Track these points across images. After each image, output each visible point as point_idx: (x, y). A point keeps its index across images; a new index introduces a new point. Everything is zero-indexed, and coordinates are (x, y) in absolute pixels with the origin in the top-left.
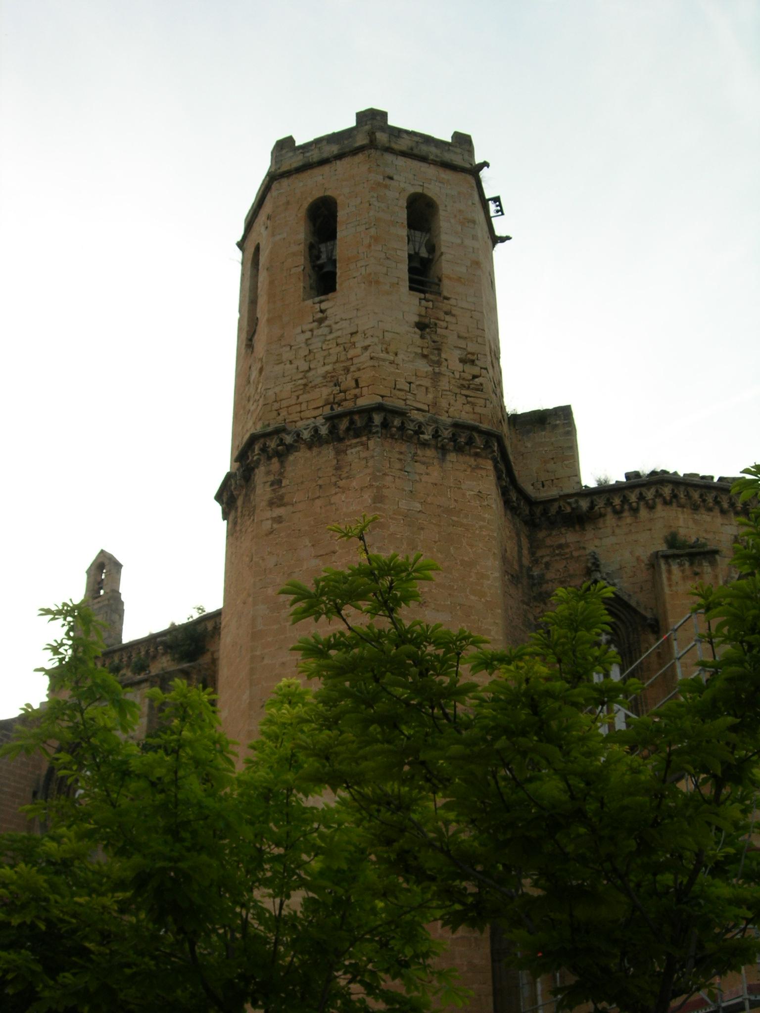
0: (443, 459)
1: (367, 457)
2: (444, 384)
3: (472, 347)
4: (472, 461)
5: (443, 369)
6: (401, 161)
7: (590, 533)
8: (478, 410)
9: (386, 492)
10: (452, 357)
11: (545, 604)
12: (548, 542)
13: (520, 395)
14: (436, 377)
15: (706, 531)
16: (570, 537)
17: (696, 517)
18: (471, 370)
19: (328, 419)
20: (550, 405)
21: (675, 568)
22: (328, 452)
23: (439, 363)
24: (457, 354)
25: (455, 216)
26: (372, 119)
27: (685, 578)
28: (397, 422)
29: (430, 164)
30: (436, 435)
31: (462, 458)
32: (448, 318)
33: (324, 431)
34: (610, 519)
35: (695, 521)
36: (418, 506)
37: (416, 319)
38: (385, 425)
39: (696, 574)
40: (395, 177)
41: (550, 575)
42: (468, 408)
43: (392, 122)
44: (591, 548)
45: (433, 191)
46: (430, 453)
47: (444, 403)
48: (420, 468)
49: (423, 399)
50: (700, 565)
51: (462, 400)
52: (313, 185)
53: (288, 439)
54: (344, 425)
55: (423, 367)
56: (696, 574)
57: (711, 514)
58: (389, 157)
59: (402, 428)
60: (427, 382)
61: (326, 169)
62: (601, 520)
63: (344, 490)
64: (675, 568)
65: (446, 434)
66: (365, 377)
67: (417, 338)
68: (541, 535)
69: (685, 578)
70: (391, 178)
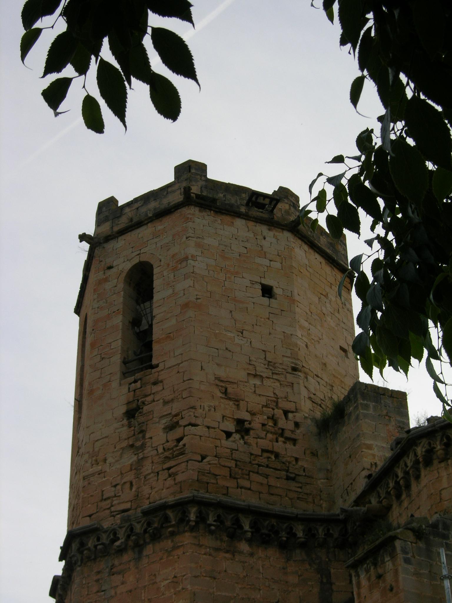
0: (139, 558)
2: (147, 467)
4: (168, 544)
10: (157, 436)
14: (140, 462)
27: (371, 588)
40: (115, 264)
48: (117, 579)
50: (383, 562)
67: (125, 431)
70: (110, 268)
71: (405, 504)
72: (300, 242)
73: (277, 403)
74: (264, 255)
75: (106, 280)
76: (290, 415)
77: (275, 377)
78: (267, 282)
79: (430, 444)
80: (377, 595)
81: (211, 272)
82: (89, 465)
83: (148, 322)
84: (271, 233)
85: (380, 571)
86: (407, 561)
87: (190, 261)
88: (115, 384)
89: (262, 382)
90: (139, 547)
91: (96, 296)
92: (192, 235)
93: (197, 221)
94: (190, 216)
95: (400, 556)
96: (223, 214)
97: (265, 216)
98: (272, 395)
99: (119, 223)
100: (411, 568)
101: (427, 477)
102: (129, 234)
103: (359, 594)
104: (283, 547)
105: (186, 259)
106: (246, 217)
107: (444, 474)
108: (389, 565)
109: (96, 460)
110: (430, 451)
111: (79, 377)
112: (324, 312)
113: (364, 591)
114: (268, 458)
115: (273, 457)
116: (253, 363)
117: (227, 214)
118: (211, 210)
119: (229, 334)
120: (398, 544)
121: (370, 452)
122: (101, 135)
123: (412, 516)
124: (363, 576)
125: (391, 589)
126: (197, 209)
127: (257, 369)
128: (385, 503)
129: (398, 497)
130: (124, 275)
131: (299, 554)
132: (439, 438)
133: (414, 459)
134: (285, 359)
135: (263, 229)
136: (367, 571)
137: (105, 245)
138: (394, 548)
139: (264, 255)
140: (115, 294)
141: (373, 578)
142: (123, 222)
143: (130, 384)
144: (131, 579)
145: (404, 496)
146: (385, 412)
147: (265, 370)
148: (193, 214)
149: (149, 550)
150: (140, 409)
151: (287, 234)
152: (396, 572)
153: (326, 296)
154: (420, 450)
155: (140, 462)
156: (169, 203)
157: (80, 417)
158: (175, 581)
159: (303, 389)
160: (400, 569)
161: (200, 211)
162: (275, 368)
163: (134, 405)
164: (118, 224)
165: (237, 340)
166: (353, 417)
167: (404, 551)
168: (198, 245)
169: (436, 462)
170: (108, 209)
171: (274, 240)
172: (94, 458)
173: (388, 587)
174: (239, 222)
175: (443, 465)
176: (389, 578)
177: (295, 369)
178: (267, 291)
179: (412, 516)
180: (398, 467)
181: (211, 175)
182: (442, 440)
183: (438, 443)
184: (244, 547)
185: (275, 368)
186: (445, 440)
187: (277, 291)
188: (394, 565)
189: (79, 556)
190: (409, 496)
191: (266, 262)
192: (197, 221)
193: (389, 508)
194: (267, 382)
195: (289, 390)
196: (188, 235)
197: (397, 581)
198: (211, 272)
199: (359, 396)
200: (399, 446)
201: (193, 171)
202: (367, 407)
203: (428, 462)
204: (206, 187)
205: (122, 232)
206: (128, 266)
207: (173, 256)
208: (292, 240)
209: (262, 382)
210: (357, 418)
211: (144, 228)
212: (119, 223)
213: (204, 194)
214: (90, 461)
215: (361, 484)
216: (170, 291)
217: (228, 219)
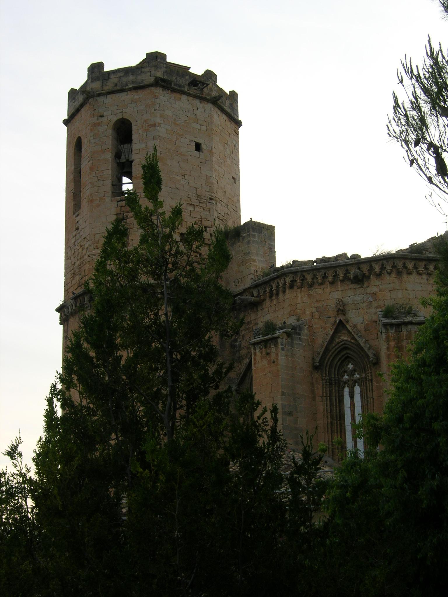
6: (109, 99)
11: (241, 364)
15: (317, 301)
17: (311, 292)
25: (142, 126)
26: (96, 70)
27: (262, 358)
29: (127, 91)
34: (267, 303)
35: (309, 296)
39: (268, 354)
40: (105, 114)
43: (77, 88)
45: (130, 114)
50: (270, 347)
52: (113, 108)
56: (268, 354)
57: (322, 286)
58: (101, 99)
62: (264, 303)
70: (102, 116)
71: (275, 302)
72: (216, 109)
73: (201, 221)
74: (197, 121)
75: (99, 124)
76: (208, 229)
77: (201, 205)
78: (198, 141)
79: (293, 277)
80: (265, 362)
81: (168, 135)
82: (92, 248)
83: (125, 158)
84: (201, 105)
85: (268, 351)
86: (283, 349)
87: (157, 128)
88: (108, 199)
89: (194, 208)
91: (92, 134)
92: (158, 109)
93: (161, 97)
94: (157, 95)
95: (280, 347)
96: (175, 92)
97: (198, 93)
98: (199, 217)
100: (284, 353)
101: (289, 294)
102: (115, 95)
103: (255, 359)
105: (155, 125)
106: (189, 95)
107: (299, 295)
108: (273, 349)
109: (97, 246)
110: (293, 281)
111: (72, 177)
112: (226, 156)
113: (258, 358)
114: (196, 256)
115: (198, 255)
116: (190, 196)
117: (177, 92)
118: (168, 90)
119: (178, 178)
120: (279, 341)
121: (255, 263)
123: (285, 323)
124: (258, 351)
125: (274, 362)
126: (161, 89)
127: (192, 200)
128: (262, 297)
129: (271, 297)
130: (112, 124)
132: (299, 275)
133: (283, 282)
134: (206, 193)
135: (197, 102)
136: (261, 349)
137: (98, 98)
138: (277, 342)
139: (197, 121)
140: (105, 136)
141: (264, 353)
142: (109, 86)
143: (118, 202)
145: (274, 298)
146: (263, 239)
147: (196, 201)
148: (159, 93)
150: (124, 219)
151: (210, 105)
152: (277, 354)
153: (227, 144)
154: (288, 280)
156: (142, 81)
159: (215, 212)
160: (279, 354)
161: (163, 91)
162: (201, 199)
163: (121, 216)
165: (182, 182)
166: (246, 241)
167: (282, 345)
168: (162, 116)
169: (295, 287)
170: (96, 70)
171: (203, 110)
172: (95, 245)
173: (272, 361)
174: (184, 98)
175: (299, 290)
176: (273, 356)
177: (211, 199)
178: (198, 147)
179: (285, 323)
180: (273, 283)
181: (168, 60)
182: (300, 277)
183: (298, 278)
185: (201, 199)
186: (302, 278)
187: (204, 147)
188: (276, 350)
189: (89, 304)
190: (277, 299)
191: (197, 126)
192: (161, 97)
193: (264, 300)
194: (197, 209)
195: (208, 213)
196: (156, 108)
197: (277, 359)
198: (168, 135)
199: (251, 229)
200: (276, 273)
201: (159, 60)
202: (254, 236)
203: (291, 287)
204: (166, 72)
205: (110, 93)
206: (115, 119)
207: (146, 121)
208: (213, 109)
209: (194, 208)
210: (249, 242)
211: (126, 93)
213: (165, 77)
214: (93, 246)
215: (248, 283)
216: (143, 146)
217: (177, 95)
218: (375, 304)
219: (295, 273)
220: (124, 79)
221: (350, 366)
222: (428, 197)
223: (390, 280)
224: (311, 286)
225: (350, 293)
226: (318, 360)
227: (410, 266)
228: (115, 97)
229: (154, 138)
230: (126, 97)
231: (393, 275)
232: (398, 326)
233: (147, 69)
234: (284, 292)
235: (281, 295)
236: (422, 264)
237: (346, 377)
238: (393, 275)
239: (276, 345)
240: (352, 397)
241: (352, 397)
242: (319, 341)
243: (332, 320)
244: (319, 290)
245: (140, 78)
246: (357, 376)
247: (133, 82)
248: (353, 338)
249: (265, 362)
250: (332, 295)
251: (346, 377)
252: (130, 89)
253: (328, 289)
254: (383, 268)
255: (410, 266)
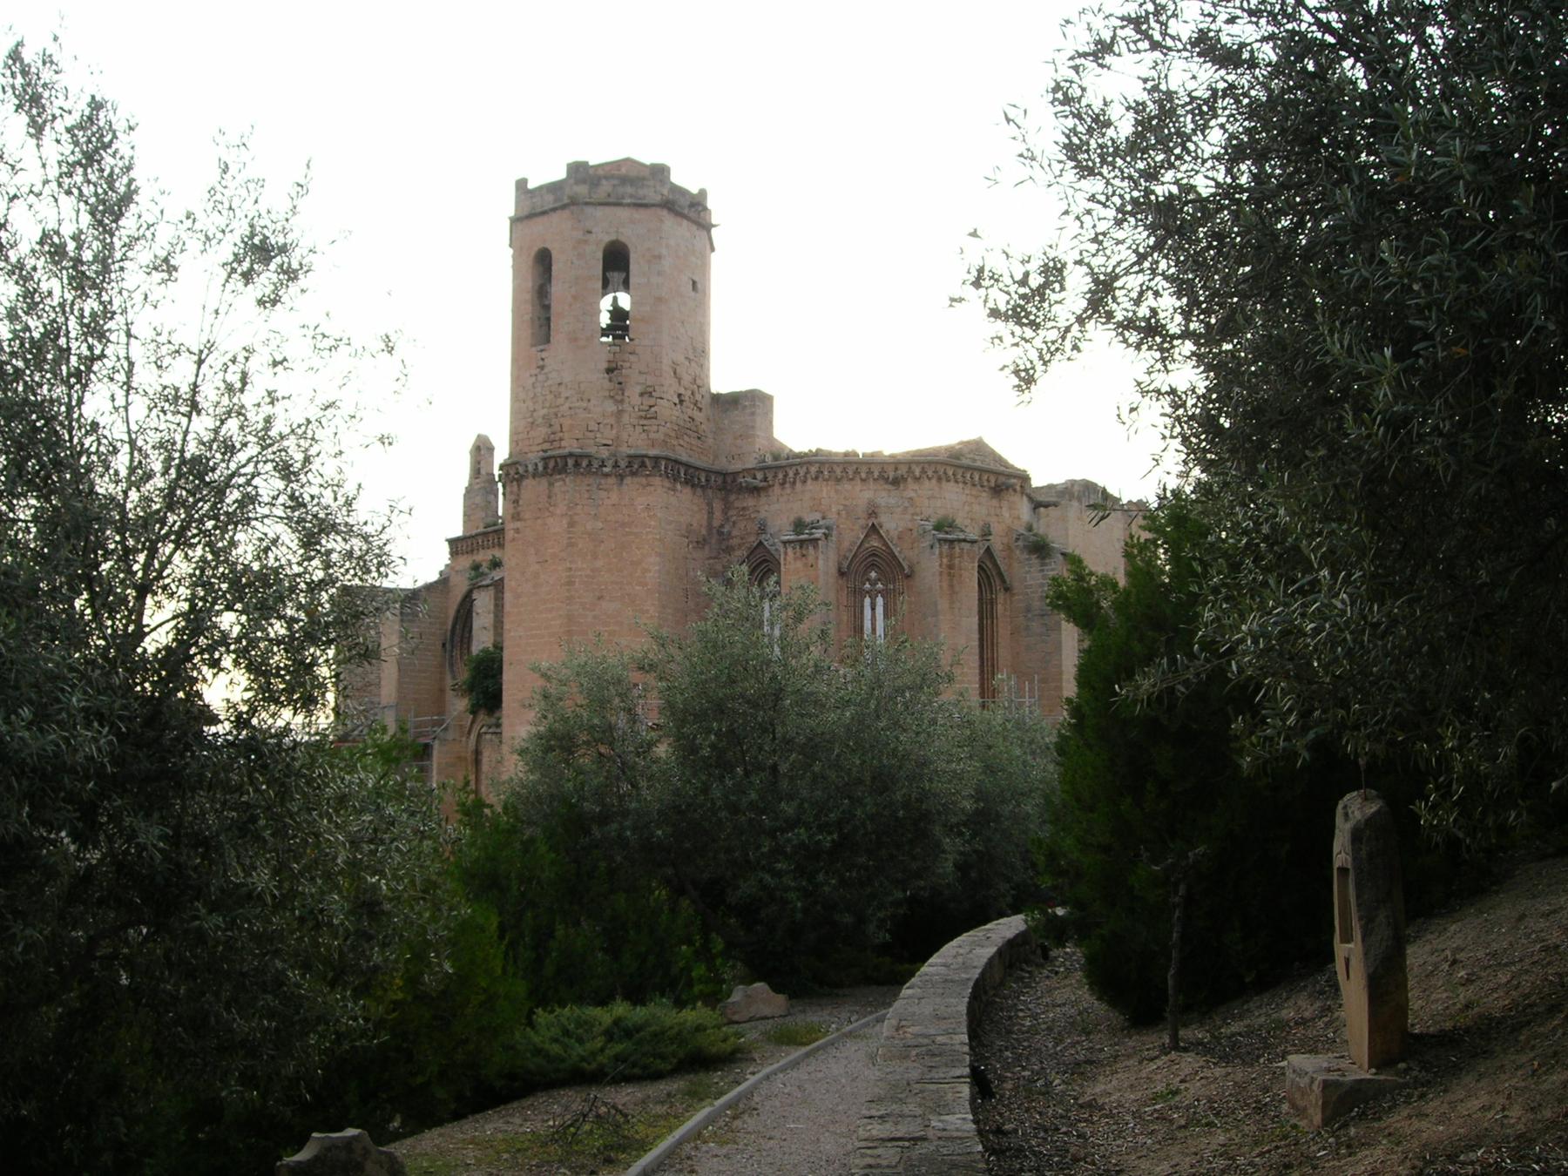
0: (621, 484)
1: (565, 487)
2: (626, 419)
3: (650, 380)
4: (644, 480)
5: (626, 406)
6: (600, 212)
7: (763, 499)
8: (652, 435)
9: (576, 518)
10: (633, 393)
12: (737, 504)
13: (723, 379)
14: (620, 412)
16: (750, 502)
18: (648, 401)
19: (544, 459)
20: (743, 389)
21: (790, 550)
22: (544, 482)
23: (622, 401)
24: (638, 389)
27: (795, 559)
28: (584, 463)
30: (616, 465)
31: (636, 480)
32: (632, 358)
33: (540, 468)
34: (777, 489)
35: (837, 491)
36: (600, 525)
37: (605, 365)
38: (577, 465)
41: (735, 533)
42: (644, 436)
44: (763, 515)
45: (628, 236)
46: (612, 480)
47: (625, 436)
48: (603, 494)
49: (608, 435)
51: (639, 429)
53: (521, 470)
54: (551, 464)
55: (611, 407)
58: (589, 210)
59: (590, 464)
60: (612, 420)
61: (545, 219)
63: (552, 514)
64: (790, 550)
65: (623, 464)
66: (567, 422)
67: (607, 384)
68: (733, 497)
69: (795, 559)
75: (586, 242)
90: (621, 477)
99: (173, 623)
104: (693, 486)
122: (483, 432)
129: (783, 484)
131: (699, 491)
144: (614, 497)
149: (628, 480)
154: (813, 469)
155: (620, 412)
157: (548, 319)
158: (648, 508)
164: (174, 618)
176: (811, 559)
184: (679, 486)
206: (607, 239)
212: (173, 623)
218: (911, 510)
219: (822, 463)
220: (621, 190)
221: (873, 574)
222: (219, 138)
223: (928, 486)
224: (838, 480)
225: (884, 494)
226: (845, 564)
227: (950, 473)
228: (607, 210)
229: (659, 273)
230: (623, 213)
231: (934, 481)
232: (951, 542)
233: (651, 183)
234: (804, 482)
235: (798, 485)
236: (960, 472)
237: (867, 585)
238: (934, 481)
239: (816, 547)
240: (873, 609)
241: (873, 609)
242: (846, 544)
243: (862, 522)
244: (848, 486)
245: (641, 192)
246: (880, 586)
247: (631, 196)
248: (886, 544)
249: (799, 564)
250: (864, 494)
251: (867, 585)
252: (629, 205)
253: (858, 486)
254: (923, 471)
255: (950, 473)
